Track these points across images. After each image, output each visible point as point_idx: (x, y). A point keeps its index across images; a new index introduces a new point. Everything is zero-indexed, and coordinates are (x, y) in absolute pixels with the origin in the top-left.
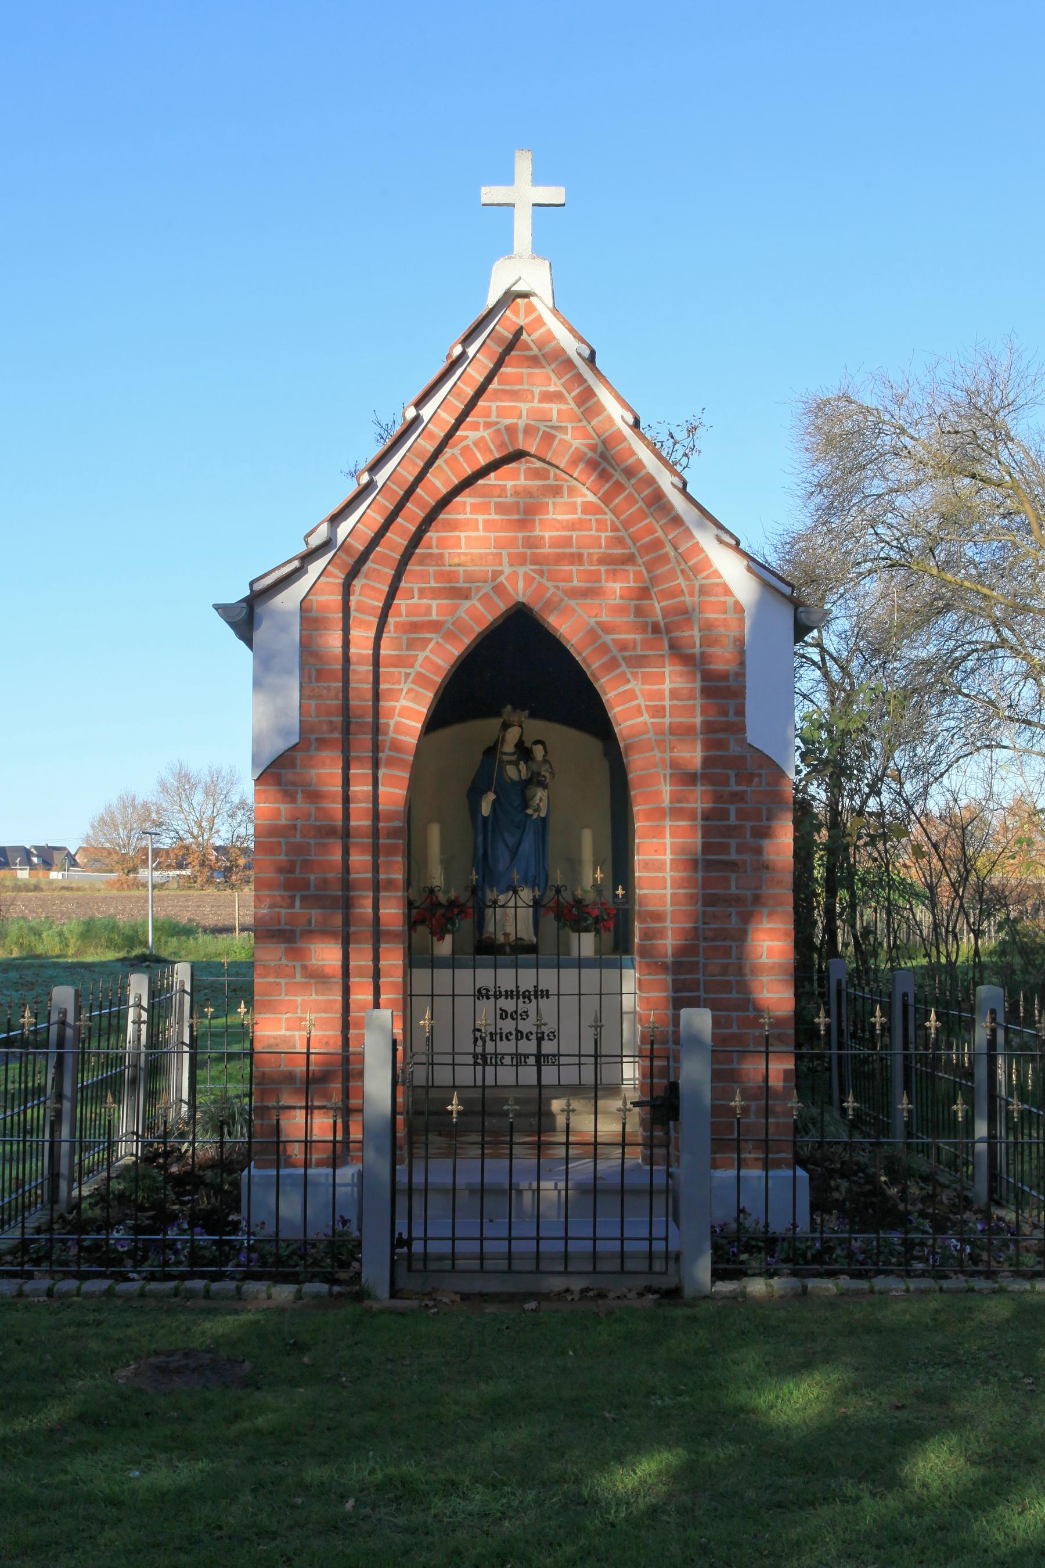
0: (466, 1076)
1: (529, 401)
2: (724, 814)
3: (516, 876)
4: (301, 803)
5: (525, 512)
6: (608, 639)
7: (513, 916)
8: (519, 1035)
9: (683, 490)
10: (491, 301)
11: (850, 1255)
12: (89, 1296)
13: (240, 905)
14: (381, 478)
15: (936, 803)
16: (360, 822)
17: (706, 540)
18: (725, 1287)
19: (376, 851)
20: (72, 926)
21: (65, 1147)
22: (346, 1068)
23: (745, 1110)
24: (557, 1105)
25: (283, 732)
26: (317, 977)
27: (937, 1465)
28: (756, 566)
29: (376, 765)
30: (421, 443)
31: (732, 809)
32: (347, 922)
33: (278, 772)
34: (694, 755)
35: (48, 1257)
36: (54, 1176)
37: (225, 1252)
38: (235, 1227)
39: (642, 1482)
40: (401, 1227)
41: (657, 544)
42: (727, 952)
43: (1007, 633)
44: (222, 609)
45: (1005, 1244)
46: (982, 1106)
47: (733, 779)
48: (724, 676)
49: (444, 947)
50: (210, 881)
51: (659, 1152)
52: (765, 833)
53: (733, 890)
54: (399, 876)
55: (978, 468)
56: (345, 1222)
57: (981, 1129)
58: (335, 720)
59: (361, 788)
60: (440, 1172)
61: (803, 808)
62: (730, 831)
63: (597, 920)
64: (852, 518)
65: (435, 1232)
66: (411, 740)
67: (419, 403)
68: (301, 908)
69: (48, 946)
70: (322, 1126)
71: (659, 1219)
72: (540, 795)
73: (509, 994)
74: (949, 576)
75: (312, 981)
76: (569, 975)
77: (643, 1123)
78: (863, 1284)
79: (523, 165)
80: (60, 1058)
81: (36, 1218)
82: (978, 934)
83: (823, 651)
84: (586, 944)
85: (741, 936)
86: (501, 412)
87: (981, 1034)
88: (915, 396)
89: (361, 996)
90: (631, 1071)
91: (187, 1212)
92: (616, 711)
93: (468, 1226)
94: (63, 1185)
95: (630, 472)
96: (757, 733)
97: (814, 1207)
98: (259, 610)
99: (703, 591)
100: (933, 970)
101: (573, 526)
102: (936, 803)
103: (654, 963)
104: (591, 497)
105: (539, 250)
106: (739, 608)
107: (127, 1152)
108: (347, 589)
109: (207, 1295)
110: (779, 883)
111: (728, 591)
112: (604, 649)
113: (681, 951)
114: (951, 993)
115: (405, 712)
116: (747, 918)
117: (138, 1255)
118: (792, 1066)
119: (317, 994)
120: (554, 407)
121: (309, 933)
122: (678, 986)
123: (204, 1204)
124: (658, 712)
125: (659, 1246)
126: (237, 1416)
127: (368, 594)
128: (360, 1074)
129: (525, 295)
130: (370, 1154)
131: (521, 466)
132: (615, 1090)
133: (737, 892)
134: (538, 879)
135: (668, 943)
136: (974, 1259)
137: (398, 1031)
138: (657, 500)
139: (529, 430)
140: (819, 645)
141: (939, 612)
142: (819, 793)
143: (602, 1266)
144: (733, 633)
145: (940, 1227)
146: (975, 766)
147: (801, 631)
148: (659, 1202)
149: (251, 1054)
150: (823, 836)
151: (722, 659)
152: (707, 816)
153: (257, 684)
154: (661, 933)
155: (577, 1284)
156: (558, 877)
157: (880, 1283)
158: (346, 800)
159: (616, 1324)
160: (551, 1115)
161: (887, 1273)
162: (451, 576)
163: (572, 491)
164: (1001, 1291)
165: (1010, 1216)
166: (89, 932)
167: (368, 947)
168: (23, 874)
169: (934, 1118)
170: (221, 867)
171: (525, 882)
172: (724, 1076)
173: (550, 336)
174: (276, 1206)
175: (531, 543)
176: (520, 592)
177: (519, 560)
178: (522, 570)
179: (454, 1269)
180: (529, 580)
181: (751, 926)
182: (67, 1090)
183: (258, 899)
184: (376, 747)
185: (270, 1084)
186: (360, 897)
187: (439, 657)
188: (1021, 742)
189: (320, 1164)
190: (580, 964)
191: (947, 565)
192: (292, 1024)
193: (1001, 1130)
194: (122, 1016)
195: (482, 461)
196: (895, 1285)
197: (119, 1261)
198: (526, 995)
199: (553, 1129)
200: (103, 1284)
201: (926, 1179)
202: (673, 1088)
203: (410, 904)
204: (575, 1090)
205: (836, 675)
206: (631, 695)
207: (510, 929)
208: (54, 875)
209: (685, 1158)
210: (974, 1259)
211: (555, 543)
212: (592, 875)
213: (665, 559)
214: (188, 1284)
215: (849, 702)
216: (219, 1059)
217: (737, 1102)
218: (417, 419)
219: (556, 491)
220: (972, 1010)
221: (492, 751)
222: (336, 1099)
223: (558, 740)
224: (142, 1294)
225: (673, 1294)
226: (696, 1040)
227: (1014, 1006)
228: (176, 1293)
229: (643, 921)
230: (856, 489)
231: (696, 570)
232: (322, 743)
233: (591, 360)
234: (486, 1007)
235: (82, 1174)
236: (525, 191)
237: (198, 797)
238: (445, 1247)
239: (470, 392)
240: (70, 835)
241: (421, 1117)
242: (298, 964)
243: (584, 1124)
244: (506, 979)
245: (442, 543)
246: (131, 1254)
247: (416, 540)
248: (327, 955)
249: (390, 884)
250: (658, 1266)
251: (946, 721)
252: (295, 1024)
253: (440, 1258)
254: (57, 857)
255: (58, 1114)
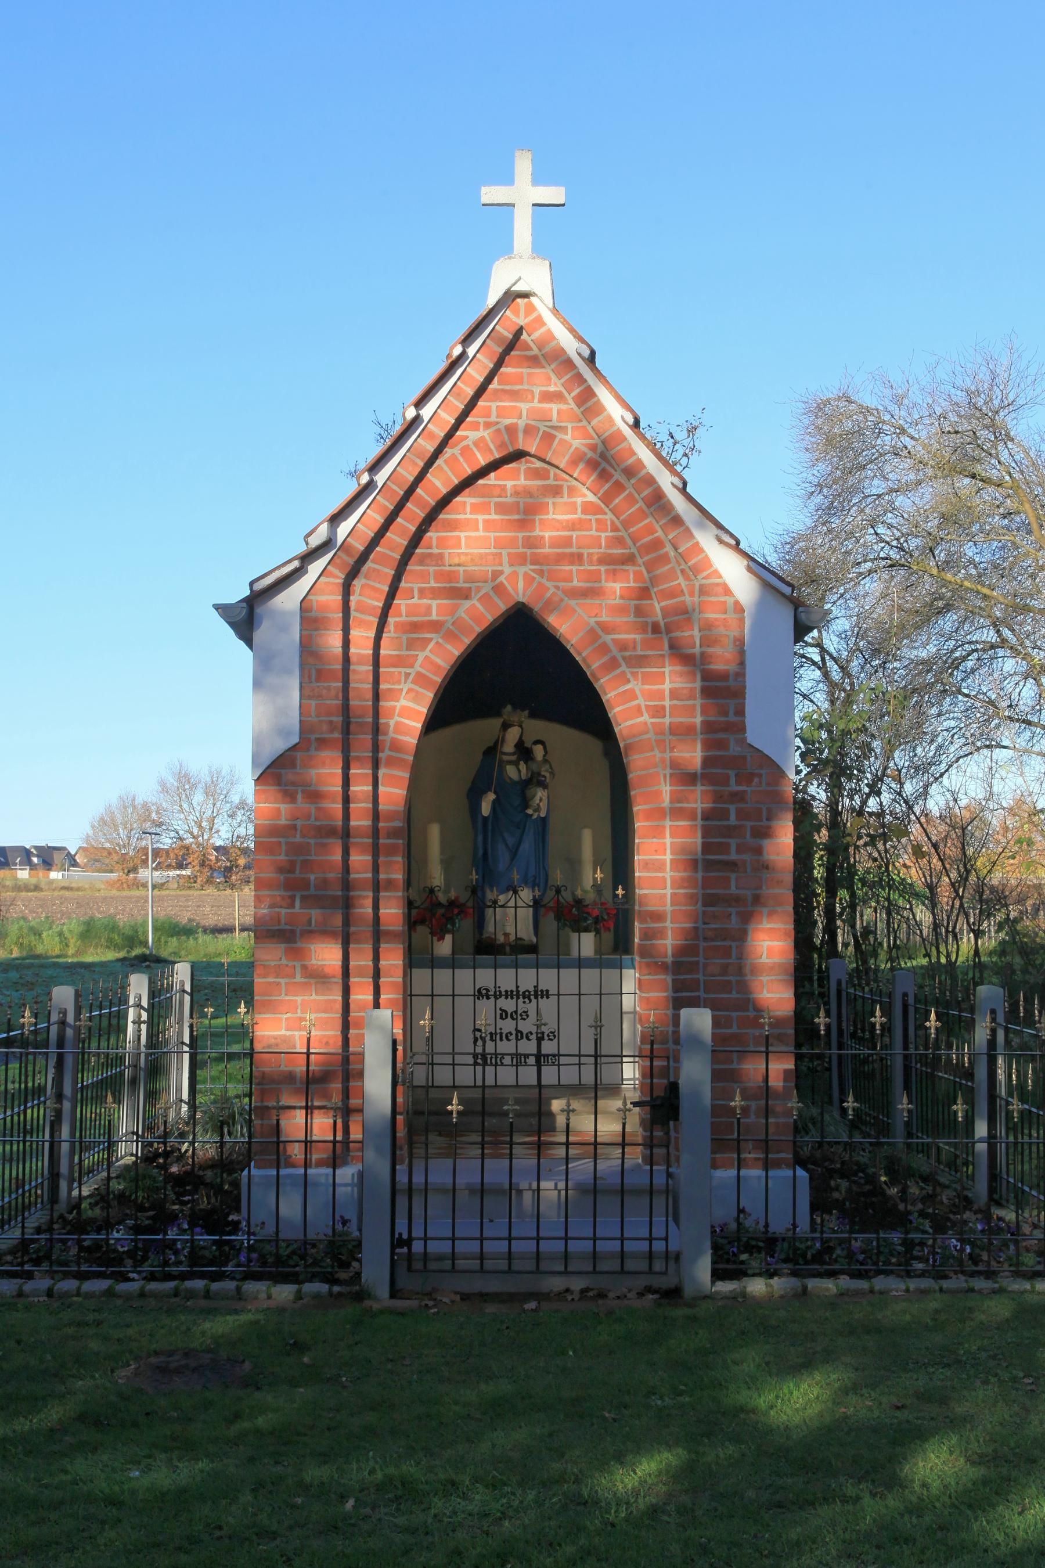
0: (466, 1076)
1: (529, 401)
2: (724, 814)
3: (516, 876)
4: (301, 803)
5: (525, 512)
6: (608, 639)
7: (513, 916)
8: (519, 1035)
9: (683, 490)
10: (491, 301)
11: (850, 1255)
12: (89, 1296)
13: (240, 905)
14: (381, 478)
15: (936, 803)
16: (360, 822)
17: (706, 540)
18: (725, 1287)
19: (376, 851)
20: (72, 926)
21: (65, 1147)
22: (346, 1068)
23: (745, 1110)
24: (557, 1105)
25: (283, 732)
26: (317, 977)
27: (937, 1465)
28: (756, 566)
29: (376, 765)
30: (421, 443)
31: (732, 809)
32: (347, 922)
33: (278, 772)
34: (694, 755)
35: (48, 1257)
36: (54, 1176)
37: (225, 1252)
38: (235, 1227)
39: (642, 1482)
40: (401, 1227)
41: (657, 544)
42: (727, 952)
43: (1007, 633)
44: (222, 609)
45: (1005, 1244)
46: (982, 1106)
47: (733, 779)
48: (724, 676)
49: (444, 947)
50: (210, 881)
51: (659, 1152)
52: (765, 833)
53: (733, 890)
54: (399, 876)
55: (978, 468)
56: (345, 1222)
57: (981, 1129)
58: (335, 720)
59: (361, 788)
60: (440, 1172)
61: (803, 808)
62: (730, 831)
63: (597, 920)
64: (852, 518)
65: (435, 1232)
66: (411, 740)
67: (419, 403)
68: (301, 908)
69: (48, 946)
70: (322, 1126)
71: (659, 1219)
72: (540, 795)
73: (509, 994)
74: (949, 576)
75: (312, 981)
76: (569, 975)
77: (643, 1123)
78: (863, 1284)
79: (523, 165)
80: (60, 1058)
81: (36, 1218)
82: (978, 934)
83: (823, 651)
84: (586, 944)
85: (741, 936)
86: (501, 412)
87: (981, 1034)
88: (915, 396)
89: (361, 996)
90: (631, 1071)
91: (187, 1212)
92: (616, 711)
93: (468, 1226)
94: (63, 1185)
95: (630, 472)
96: (757, 733)
97: (814, 1207)
98: (259, 610)
99: (703, 591)
100: (933, 970)
101: (573, 526)
102: (936, 803)
103: (654, 963)
104: (591, 497)
105: (539, 250)
106: (739, 608)
107: (127, 1152)
108: (347, 589)
109: (207, 1295)
110: (779, 883)
111: (728, 591)
112: (604, 649)
113: (681, 951)
114: (951, 993)
115: (405, 712)
116: (747, 918)
117: (138, 1255)
118: (792, 1066)
119: (317, 994)
120: (554, 407)
121: (309, 933)
122: (678, 986)
123: (204, 1204)
124: (658, 712)
125: (659, 1246)
126: (237, 1416)
127: (368, 594)
128: (360, 1074)
129: (525, 295)
130: (370, 1154)
131: (521, 466)
132: (615, 1090)
133: (737, 892)
134: (538, 879)
135: (668, 943)
136: (974, 1259)
137: (398, 1031)
138: (657, 500)
139: (529, 430)
140: (819, 645)
141: (939, 612)
142: (819, 793)
143: (602, 1266)
144: (733, 633)
145: (940, 1227)
146: (975, 766)
147: (801, 631)
148: (659, 1202)
149: (251, 1054)
150: (823, 836)
151: (722, 659)
152: (707, 816)
153: (257, 684)
154: (661, 933)
155: (577, 1284)
156: (558, 877)
157: (880, 1283)
158: (346, 800)
159: (616, 1324)
160: (551, 1115)
161: (887, 1273)
162: (451, 576)
163: (572, 491)
164: (1001, 1291)
165: (1010, 1216)
166: (89, 932)
167: (368, 947)
168: (23, 874)
169: (934, 1118)
170: (221, 867)
171: (525, 882)
172: (724, 1076)
173: (550, 336)
174: (276, 1206)
175: (531, 543)
176: (520, 592)
177: (519, 560)
178: (522, 570)
179: (454, 1269)
180: (529, 580)
181: (751, 926)
182: (67, 1090)
183: (258, 899)
184: (376, 747)
185: (270, 1084)
186: (360, 897)
187: (439, 657)
188: (1021, 742)
189: (320, 1164)
190: (580, 964)
191: (947, 565)
192: (292, 1024)
193: (1001, 1130)
194: (122, 1016)
195: (482, 461)
196: (895, 1285)
197: (119, 1261)
198: (526, 995)
199: (553, 1129)
200: (103, 1284)
201: (926, 1179)
202: (673, 1088)
203: (410, 904)
204: (575, 1090)
205: (836, 675)
206: (631, 695)
207: (510, 929)
208: (54, 875)
209: (685, 1158)
210: (974, 1259)
211: (555, 543)
212: (592, 875)
213: (665, 559)
214: (188, 1284)
215: (849, 702)
216: (219, 1059)
217: (737, 1102)
218: (417, 419)
219: (556, 491)
220: (972, 1010)
221: (492, 751)
222: (336, 1099)
223: (558, 740)
224: (142, 1294)
225: (673, 1294)
226: (696, 1040)
227: (1014, 1006)
228: (176, 1293)
229: (643, 921)
230: (856, 489)
231: (696, 570)
232: (322, 743)
233: (591, 360)
234: (486, 1007)
235: (82, 1174)
236: (525, 191)
237: (198, 797)
238: (445, 1247)
239: (470, 392)
240: (70, 835)
241: (421, 1117)
242: (298, 964)
243: (584, 1124)
244: (506, 979)
245: (442, 543)
246: (131, 1254)
247: (416, 540)
248: (327, 955)
249: (390, 884)
250: (658, 1266)
251: (946, 721)
252: (295, 1024)
253: (440, 1258)
254: (57, 857)
255: (58, 1114)
